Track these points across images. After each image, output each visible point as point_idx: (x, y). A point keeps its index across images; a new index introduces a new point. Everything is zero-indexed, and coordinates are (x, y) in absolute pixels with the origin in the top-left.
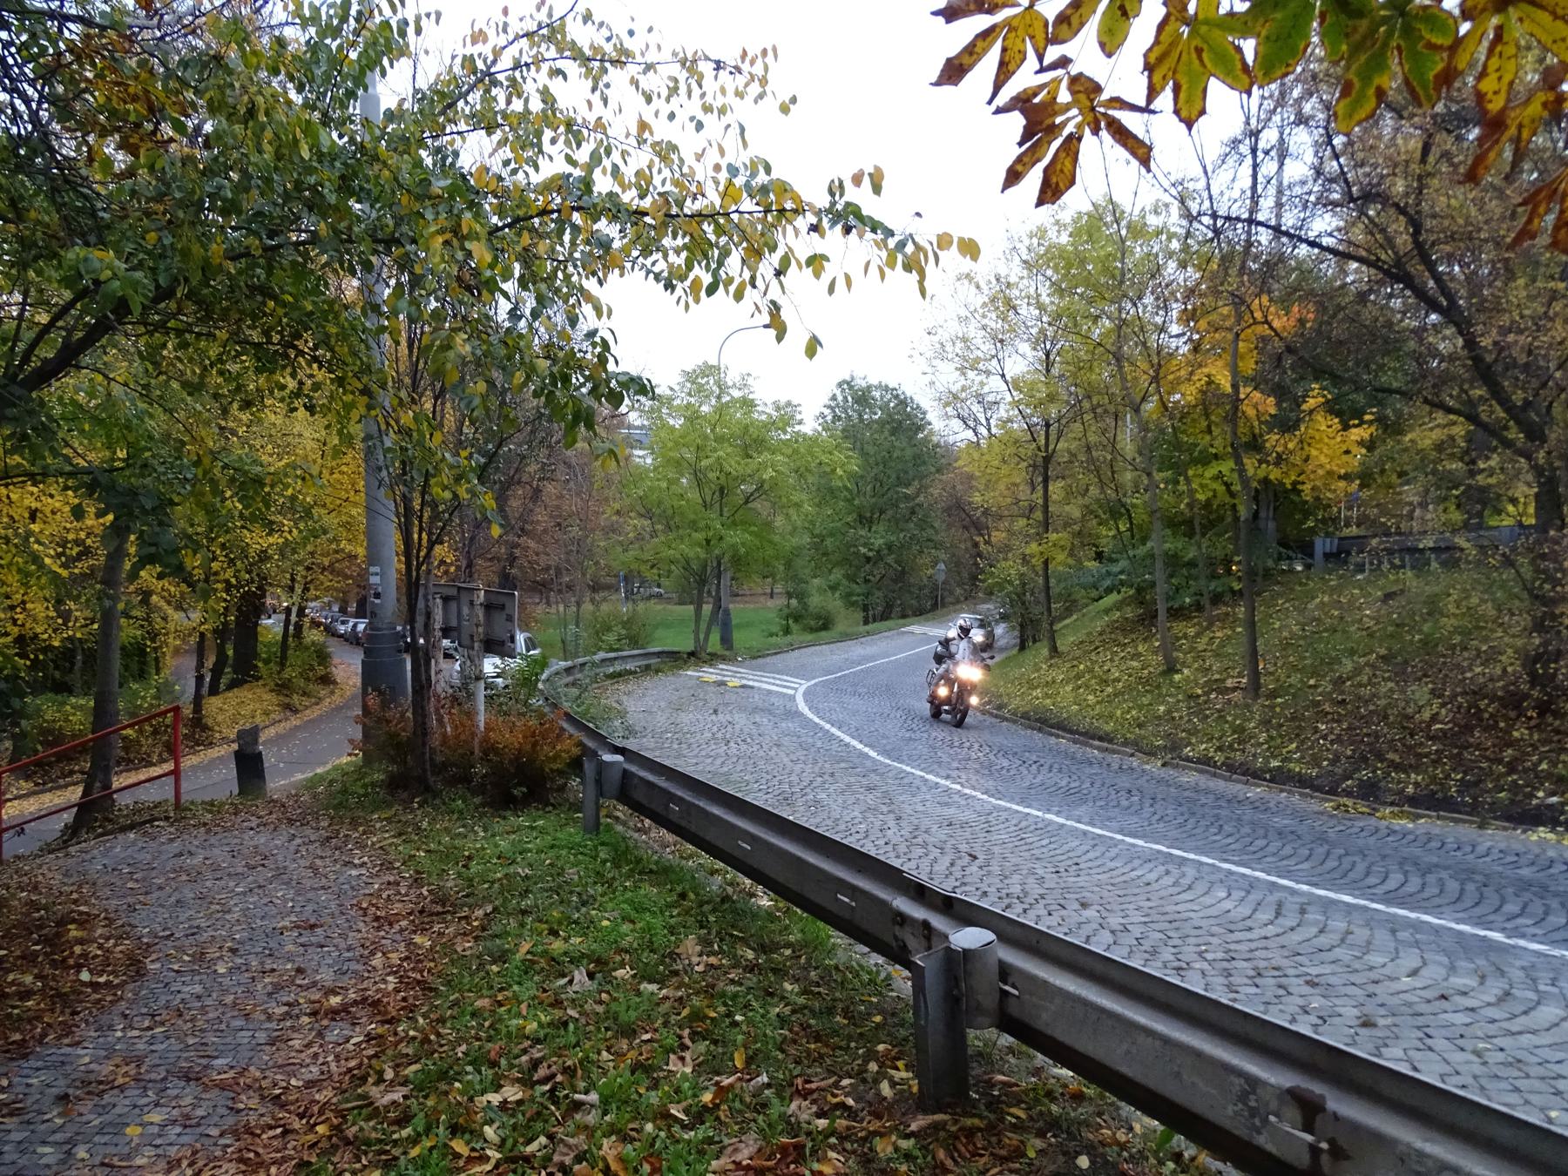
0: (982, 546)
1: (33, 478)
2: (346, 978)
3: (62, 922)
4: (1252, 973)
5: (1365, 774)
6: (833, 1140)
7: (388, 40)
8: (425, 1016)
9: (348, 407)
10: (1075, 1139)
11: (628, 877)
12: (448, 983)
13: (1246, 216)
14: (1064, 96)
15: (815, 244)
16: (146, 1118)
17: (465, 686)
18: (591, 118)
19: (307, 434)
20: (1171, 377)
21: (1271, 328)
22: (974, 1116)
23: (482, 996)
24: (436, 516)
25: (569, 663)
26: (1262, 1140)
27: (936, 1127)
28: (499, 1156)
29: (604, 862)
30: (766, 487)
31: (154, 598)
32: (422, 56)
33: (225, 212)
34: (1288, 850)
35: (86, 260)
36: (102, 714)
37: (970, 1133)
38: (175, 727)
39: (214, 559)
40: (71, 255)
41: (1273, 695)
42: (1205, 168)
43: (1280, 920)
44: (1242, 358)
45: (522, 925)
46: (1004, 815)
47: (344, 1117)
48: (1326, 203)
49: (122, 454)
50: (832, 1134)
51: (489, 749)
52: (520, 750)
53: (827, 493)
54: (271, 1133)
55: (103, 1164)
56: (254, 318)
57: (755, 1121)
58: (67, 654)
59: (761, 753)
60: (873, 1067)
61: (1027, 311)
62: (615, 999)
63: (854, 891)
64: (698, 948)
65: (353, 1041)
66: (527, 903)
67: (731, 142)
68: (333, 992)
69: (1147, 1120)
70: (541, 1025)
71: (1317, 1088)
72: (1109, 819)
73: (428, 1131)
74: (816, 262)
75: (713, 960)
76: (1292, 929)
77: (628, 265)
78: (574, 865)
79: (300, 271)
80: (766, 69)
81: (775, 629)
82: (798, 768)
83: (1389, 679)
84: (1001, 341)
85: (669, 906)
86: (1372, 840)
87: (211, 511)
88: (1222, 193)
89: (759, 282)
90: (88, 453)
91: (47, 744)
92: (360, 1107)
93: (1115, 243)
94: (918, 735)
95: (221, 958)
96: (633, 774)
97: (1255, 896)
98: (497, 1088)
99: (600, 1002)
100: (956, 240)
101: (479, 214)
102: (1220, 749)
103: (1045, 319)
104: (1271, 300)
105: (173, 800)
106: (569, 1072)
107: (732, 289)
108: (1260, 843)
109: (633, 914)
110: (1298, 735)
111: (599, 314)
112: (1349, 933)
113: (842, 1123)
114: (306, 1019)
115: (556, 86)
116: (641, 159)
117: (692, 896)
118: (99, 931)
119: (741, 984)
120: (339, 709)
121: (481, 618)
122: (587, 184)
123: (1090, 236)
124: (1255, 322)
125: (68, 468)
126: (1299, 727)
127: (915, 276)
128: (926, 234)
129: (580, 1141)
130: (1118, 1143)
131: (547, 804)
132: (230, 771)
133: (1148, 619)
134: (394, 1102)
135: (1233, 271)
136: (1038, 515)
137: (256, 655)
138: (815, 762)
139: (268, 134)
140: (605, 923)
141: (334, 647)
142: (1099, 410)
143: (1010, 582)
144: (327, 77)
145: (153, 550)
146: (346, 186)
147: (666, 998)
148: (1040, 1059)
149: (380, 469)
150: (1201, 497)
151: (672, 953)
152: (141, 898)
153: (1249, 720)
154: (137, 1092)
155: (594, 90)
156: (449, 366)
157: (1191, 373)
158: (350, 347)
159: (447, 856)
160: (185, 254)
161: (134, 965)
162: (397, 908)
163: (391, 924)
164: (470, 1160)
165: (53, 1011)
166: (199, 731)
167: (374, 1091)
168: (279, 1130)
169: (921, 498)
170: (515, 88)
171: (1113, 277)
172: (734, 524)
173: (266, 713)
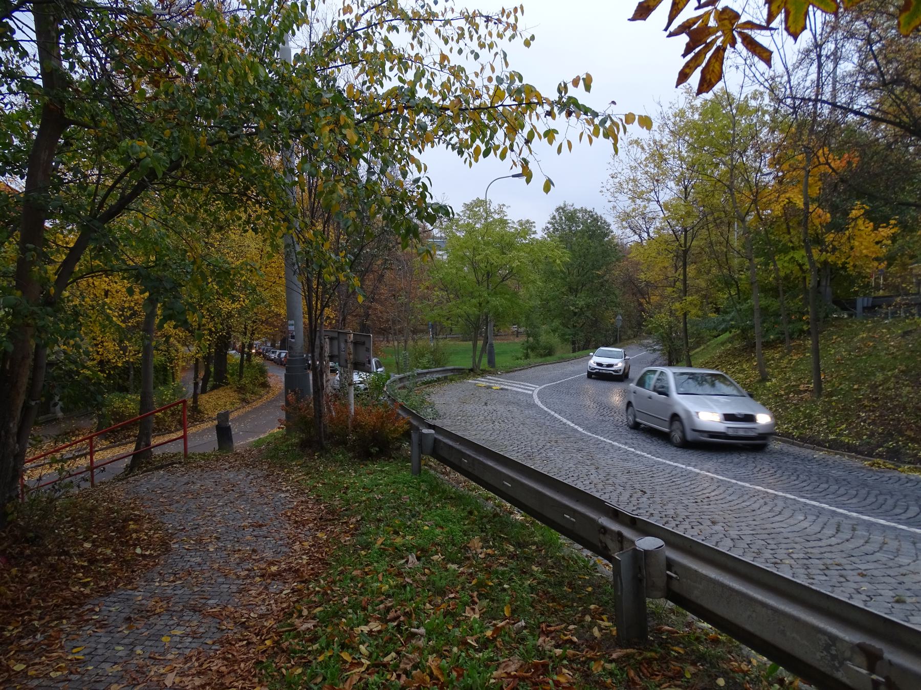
0: (645, 305)
1: (107, 273)
2: (280, 555)
3: (126, 520)
4: (823, 567)
5: (891, 444)
6: (565, 662)
7: (296, 14)
8: (324, 579)
9: (277, 229)
10: (715, 667)
11: (438, 502)
12: (337, 561)
13: (813, 97)
14: (712, 23)
15: (551, 123)
16: (173, 632)
17: (342, 386)
18: (413, 54)
19: (252, 246)
20: (764, 200)
21: (830, 167)
22: (651, 651)
23: (356, 569)
24: (325, 292)
25: (402, 375)
26: (839, 675)
27: (628, 656)
28: (368, 663)
29: (424, 492)
30: (514, 271)
31: (172, 339)
32: (315, 25)
33: (207, 118)
34: (842, 490)
35: (132, 146)
36: (145, 404)
37: (649, 661)
38: (184, 412)
39: (203, 317)
40: (123, 144)
41: (830, 395)
42: (787, 69)
43: (839, 535)
44: (810, 187)
45: (378, 528)
46: (662, 467)
47: (280, 636)
48: (866, 88)
49: (153, 258)
50: (565, 658)
51: (357, 425)
52: (374, 426)
53: (550, 274)
54: (240, 644)
55: (150, 658)
56: (223, 178)
57: (518, 648)
58: (125, 370)
59: (514, 429)
60: (588, 618)
61: (673, 162)
62: (433, 573)
63: (574, 512)
64: (481, 544)
65: (285, 592)
66: (381, 515)
67: (498, 63)
68: (272, 563)
69: (760, 657)
70: (390, 587)
71: (877, 644)
72: (727, 470)
73: (328, 646)
74: (550, 134)
75: (489, 551)
76: (847, 541)
77: (436, 140)
78: (407, 493)
79: (249, 151)
80: (516, 20)
81: (520, 355)
82: (535, 438)
83: (907, 385)
84: (657, 181)
85: (463, 518)
86: (896, 486)
87: (201, 290)
88: (799, 84)
89: (515, 147)
90: (135, 258)
91: (116, 420)
92: (290, 631)
93: (729, 118)
94: (607, 418)
95: (211, 542)
96: (440, 441)
97: (822, 519)
98: (367, 623)
99: (424, 574)
100: (637, 117)
101: (350, 115)
102: (796, 428)
103: (684, 166)
104: (830, 150)
105: (183, 452)
106: (408, 615)
107: (499, 152)
108: (825, 486)
109: (442, 523)
110: (847, 420)
111: (419, 170)
112: (884, 543)
113: (571, 652)
114: (258, 579)
115: (393, 37)
116: (441, 77)
117: (476, 513)
118: (145, 526)
119: (506, 566)
120: (271, 402)
122: (413, 92)
123: (713, 115)
124: (820, 164)
125: (124, 267)
126: (847, 415)
127: (611, 140)
128: (618, 113)
129: (415, 656)
130: (742, 671)
131: (391, 457)
132: (213, 437)
133: (750, 347)
134: (308, 629)
135: (806, 132)
136: (679, 285)
137: (226, 371)
138: (546, 434)
139: (230, 71)
140: (426, 528)
141: (269, 367)
142: (718, 221)
143: (662, 326)
144: (262, 37)
145: (171, 312)
146: (274, 100)
147: (463, 573)
148: (690, 617)
149: (294, 264)
150: (782, 274)
151: (465, 546)
152: (168, 507)
153: (815, 410)
154: (167, 617)
155: (413, 38)
156: (334, 202)
157: (779, 197)
158: (277, 194)
159: (335, 486)
160: (186, 141)
161: (165, 546)
162: (307, 516)
163: (304, 526)
164: (352, 664)
165: (122, 570)
166: (196, 414)
167: (297, 622)
168: (245, 642)
169: (607, 277)
170: (369, 39)
171: (728, 139)
172: (496, 293)
173: (232, 404)
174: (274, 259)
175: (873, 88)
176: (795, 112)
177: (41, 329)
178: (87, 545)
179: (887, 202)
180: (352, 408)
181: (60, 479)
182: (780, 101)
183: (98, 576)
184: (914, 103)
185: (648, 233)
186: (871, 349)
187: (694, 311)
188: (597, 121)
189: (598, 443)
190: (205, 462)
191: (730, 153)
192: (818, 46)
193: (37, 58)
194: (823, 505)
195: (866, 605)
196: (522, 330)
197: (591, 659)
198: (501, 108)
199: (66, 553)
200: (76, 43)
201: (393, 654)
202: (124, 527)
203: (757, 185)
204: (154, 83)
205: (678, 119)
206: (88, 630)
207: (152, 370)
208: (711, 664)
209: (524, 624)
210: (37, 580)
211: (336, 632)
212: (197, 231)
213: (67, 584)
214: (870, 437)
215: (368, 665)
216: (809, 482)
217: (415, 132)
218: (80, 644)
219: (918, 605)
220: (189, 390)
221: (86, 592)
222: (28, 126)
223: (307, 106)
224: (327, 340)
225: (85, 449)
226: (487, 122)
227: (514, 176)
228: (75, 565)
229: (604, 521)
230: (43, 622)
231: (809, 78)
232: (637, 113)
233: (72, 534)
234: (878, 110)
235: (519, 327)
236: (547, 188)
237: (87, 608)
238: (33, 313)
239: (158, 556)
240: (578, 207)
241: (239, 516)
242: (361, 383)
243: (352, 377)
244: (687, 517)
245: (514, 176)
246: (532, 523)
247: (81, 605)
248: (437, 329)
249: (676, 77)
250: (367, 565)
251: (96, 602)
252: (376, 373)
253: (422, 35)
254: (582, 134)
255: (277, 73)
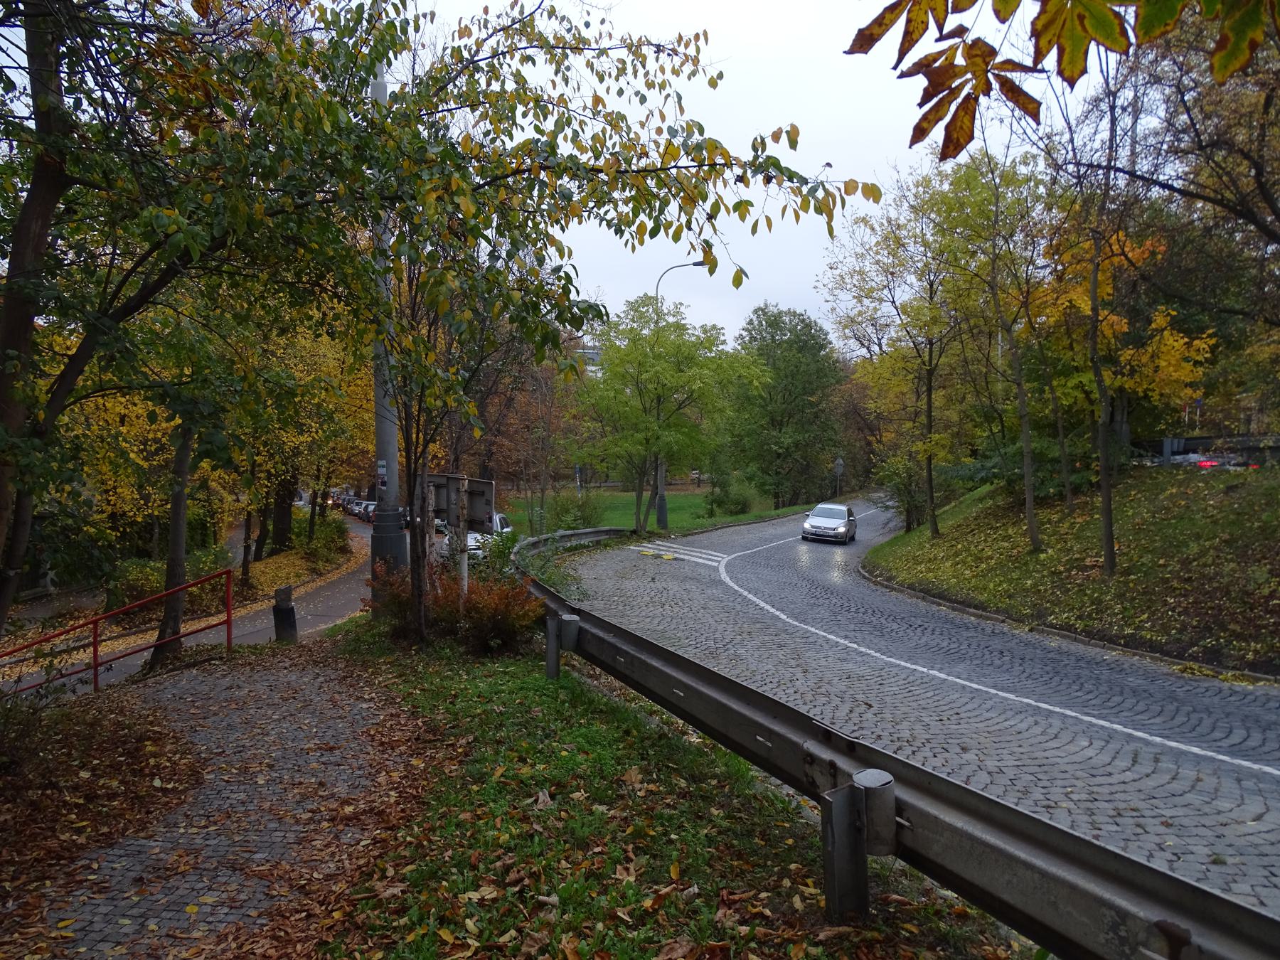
1: (125, 390)
3: (141, 739)
4: (1114, 813)
5: (1209, 642)
6: (753, 945)
7: (393, 37)
8: (419, 825)
9: (361, 334)
10: (961, 954)
11: (582, 716)
12: (438, 799)
13: (1104, 164)
14: (960, 60)
15: (744, 193)
16: (202, 900)
19: (330, 355)
22: (873, 929)
23: (464, 811)
24: (430, 420)
25: (535, 539)
27: (841, 937)
28: (477, 944)
29: (563, 702)
30: (695, 395)
32: (420, 52)
33: (264, 177)
34: (1141, 707)
35: (157, 217)
36: (173, 575)
37: (870, 944)
40: (145, 213)
41: (1127, 572)
42: (1068, 124)
43: (1137, 767)
45: (497, 753)
46: (895, 670)
47: (355, 906)
48: (1175, 151)
49: (187, 371)
50: (752, 940)
51: (471, 608)
52: (496, 610)
53: (745, 401)
54: (297, 916)
55: (168, 936)
56: (288, 262)
57: (687, 925)
58: (148, 527)
59: (691, 615)
62: (572, 817)
63: (770, 734)
64: (640, 777)
65: (362, 843)
66: (502, 734)
67: (671, 109)
68: (347, 802)
69: (1023, 939)
70: (512, 836)
71: (1182, 923)
72: (985, 676)
73: (421, 920)
74: (742, 207)
75: (652, 787)
77: (586, 214)
78: (539, 705)
79: (324, 225)
81: (701, 512)
82: (721, 627)
83: (1232, 560)
84: (892, 274)
85: (616, 741)
86: (1216, 700)
87: (255, 416)
88: (1085, 145)
89: (694, 225)
92: (367, 898)
96: (587, 631)
97: (1113, 746)
98: (477, 888)
99: (560, 819)
101: (465, 176)
102: (1080, 618)
103: (929, 254)
105: (225, 644)
106: (535, 876)
107: (671, 231)
108: (1117, 699)
109: (587, 747)
110: (1149, 607)
111: (562, 256)
112: (1199, 780)
113: (760, 930)
114: (325, 824)
115: (527, 70)
117: (635, 732)
118: (169, 747)
119: (675, 808)
120: (353, 573)
122: (552, 147)
126: (1150, 600)
128: (835, 180)
129: (543, 935)
131: (517, 654)
132: (269, 622)
133: (1017, 506)
134: (394, 896)
137: (290, 530)
138: (736, 623)
139: (298, 114)
140: (564, 753)
143: (897, 475)
144: (346, 68)
145: (209, 446)
146: (360, 155)
147: (614, 817)
148: (929, 882)
151: (619, 780)
152: (201, 722)
154: (195, 878)
155: (556, 73)
158: (363, 284)
159: (437, 694)
160: (234, 210)
161: (195, 776)
162: (398, 735)
163: (393, 749)
164: (454, 946)
165: (132, 810)
166: (247, 589)
167: (379, 886)
168: (304, 914)
170: (494, 73)
171: (988, 219)
172: (669, 426)
173: (298, 576)
174: (361, 375)
175: (1186, 152)
176: (1080, 183)
177: (26, 470)
178: (85, 775)
179: (1204, 307)
180: (465, 583)
181: (48, 681)
182: (1058, 168)
183: (98, 819)
184: (1240, 174)
185: (880, 346)
186: (1182, 510)
187: (942, 454)
188: (805, 190)
189: (806, 635)
190: (257, 658)
191: (992, 238)
192: (1111, 94)
193: (29, 91)
194: (1116, 726)
195: (1172, 869)
196: (705, 476)
197: (789, 941)
198: (674, 171)
199: (54, 786)
200: (84, 71)
201: (513, 933)
202: (137, 749)
203: (1028, 281)
204: (190, 127)
205: (921, 189)
206: (82, 895)
207: (184, 530)
208: (956, 948)
209: (697, 890)
210: (12, 823)
211: (433, 901)
212: (251, 333)
213: (53, 830)
214: (1180, 631)
215: (477, 948)
216: (1096, 693)
217: (556, 203)
218: (69, 914)
219: (1242, 867)
220: (237, 556)
221: (80, 841)
222: (14, 186)
223: (406, 164)
224: (432, 488)
225: (87, 637)
226: (655, 190)
227: (695, 264)
228: (65, 803)
229: (811, 746)
230: (17, 883)
231: (1098, 137)
232: (861, 179)
233: (63, 758)
234: (1192, 182)
235: (701, 473)
236: (738, 280)
237: (80, 863)
238: (13, 447)
239: (186, 790)
240: (784, 308)
241: (303, 735)
242: (479, 548)
243: (466, 540)
244: (928, 741)
245: (695, 264)
246: (714, 748)
247: (72, 860)
248: (587, 475)
249: (909, 133)
250: (480, 806)
251: (94, 856)
252: (500, 534)
253: (568, 69)
254: (785, 208)
255: (364, 118)
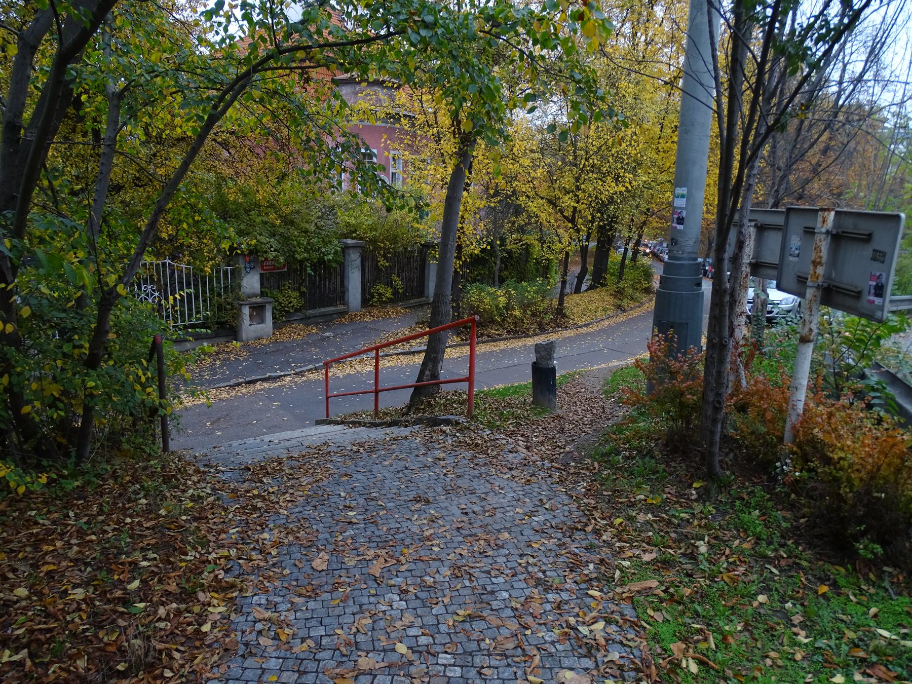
121: (824, 253)
137: (605, 270)
173: (605, 310)
180: (801, 396)
